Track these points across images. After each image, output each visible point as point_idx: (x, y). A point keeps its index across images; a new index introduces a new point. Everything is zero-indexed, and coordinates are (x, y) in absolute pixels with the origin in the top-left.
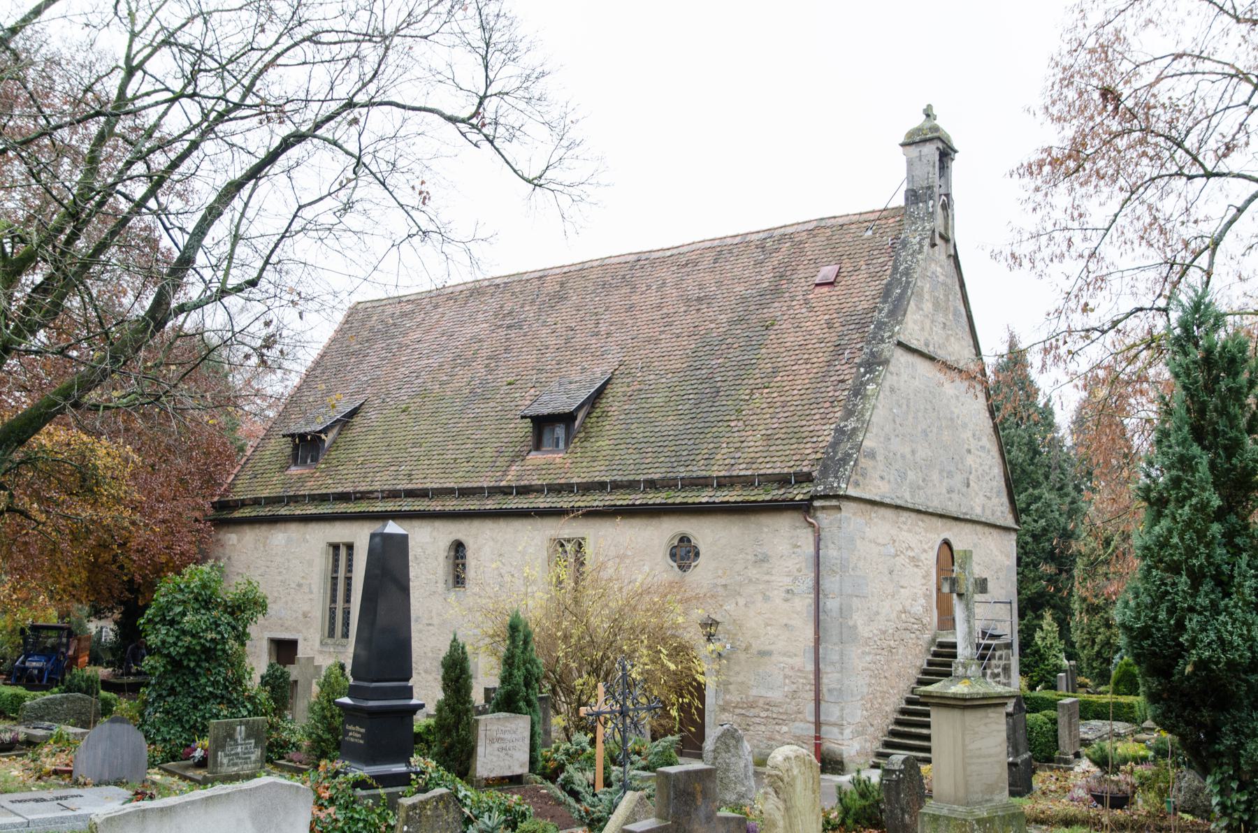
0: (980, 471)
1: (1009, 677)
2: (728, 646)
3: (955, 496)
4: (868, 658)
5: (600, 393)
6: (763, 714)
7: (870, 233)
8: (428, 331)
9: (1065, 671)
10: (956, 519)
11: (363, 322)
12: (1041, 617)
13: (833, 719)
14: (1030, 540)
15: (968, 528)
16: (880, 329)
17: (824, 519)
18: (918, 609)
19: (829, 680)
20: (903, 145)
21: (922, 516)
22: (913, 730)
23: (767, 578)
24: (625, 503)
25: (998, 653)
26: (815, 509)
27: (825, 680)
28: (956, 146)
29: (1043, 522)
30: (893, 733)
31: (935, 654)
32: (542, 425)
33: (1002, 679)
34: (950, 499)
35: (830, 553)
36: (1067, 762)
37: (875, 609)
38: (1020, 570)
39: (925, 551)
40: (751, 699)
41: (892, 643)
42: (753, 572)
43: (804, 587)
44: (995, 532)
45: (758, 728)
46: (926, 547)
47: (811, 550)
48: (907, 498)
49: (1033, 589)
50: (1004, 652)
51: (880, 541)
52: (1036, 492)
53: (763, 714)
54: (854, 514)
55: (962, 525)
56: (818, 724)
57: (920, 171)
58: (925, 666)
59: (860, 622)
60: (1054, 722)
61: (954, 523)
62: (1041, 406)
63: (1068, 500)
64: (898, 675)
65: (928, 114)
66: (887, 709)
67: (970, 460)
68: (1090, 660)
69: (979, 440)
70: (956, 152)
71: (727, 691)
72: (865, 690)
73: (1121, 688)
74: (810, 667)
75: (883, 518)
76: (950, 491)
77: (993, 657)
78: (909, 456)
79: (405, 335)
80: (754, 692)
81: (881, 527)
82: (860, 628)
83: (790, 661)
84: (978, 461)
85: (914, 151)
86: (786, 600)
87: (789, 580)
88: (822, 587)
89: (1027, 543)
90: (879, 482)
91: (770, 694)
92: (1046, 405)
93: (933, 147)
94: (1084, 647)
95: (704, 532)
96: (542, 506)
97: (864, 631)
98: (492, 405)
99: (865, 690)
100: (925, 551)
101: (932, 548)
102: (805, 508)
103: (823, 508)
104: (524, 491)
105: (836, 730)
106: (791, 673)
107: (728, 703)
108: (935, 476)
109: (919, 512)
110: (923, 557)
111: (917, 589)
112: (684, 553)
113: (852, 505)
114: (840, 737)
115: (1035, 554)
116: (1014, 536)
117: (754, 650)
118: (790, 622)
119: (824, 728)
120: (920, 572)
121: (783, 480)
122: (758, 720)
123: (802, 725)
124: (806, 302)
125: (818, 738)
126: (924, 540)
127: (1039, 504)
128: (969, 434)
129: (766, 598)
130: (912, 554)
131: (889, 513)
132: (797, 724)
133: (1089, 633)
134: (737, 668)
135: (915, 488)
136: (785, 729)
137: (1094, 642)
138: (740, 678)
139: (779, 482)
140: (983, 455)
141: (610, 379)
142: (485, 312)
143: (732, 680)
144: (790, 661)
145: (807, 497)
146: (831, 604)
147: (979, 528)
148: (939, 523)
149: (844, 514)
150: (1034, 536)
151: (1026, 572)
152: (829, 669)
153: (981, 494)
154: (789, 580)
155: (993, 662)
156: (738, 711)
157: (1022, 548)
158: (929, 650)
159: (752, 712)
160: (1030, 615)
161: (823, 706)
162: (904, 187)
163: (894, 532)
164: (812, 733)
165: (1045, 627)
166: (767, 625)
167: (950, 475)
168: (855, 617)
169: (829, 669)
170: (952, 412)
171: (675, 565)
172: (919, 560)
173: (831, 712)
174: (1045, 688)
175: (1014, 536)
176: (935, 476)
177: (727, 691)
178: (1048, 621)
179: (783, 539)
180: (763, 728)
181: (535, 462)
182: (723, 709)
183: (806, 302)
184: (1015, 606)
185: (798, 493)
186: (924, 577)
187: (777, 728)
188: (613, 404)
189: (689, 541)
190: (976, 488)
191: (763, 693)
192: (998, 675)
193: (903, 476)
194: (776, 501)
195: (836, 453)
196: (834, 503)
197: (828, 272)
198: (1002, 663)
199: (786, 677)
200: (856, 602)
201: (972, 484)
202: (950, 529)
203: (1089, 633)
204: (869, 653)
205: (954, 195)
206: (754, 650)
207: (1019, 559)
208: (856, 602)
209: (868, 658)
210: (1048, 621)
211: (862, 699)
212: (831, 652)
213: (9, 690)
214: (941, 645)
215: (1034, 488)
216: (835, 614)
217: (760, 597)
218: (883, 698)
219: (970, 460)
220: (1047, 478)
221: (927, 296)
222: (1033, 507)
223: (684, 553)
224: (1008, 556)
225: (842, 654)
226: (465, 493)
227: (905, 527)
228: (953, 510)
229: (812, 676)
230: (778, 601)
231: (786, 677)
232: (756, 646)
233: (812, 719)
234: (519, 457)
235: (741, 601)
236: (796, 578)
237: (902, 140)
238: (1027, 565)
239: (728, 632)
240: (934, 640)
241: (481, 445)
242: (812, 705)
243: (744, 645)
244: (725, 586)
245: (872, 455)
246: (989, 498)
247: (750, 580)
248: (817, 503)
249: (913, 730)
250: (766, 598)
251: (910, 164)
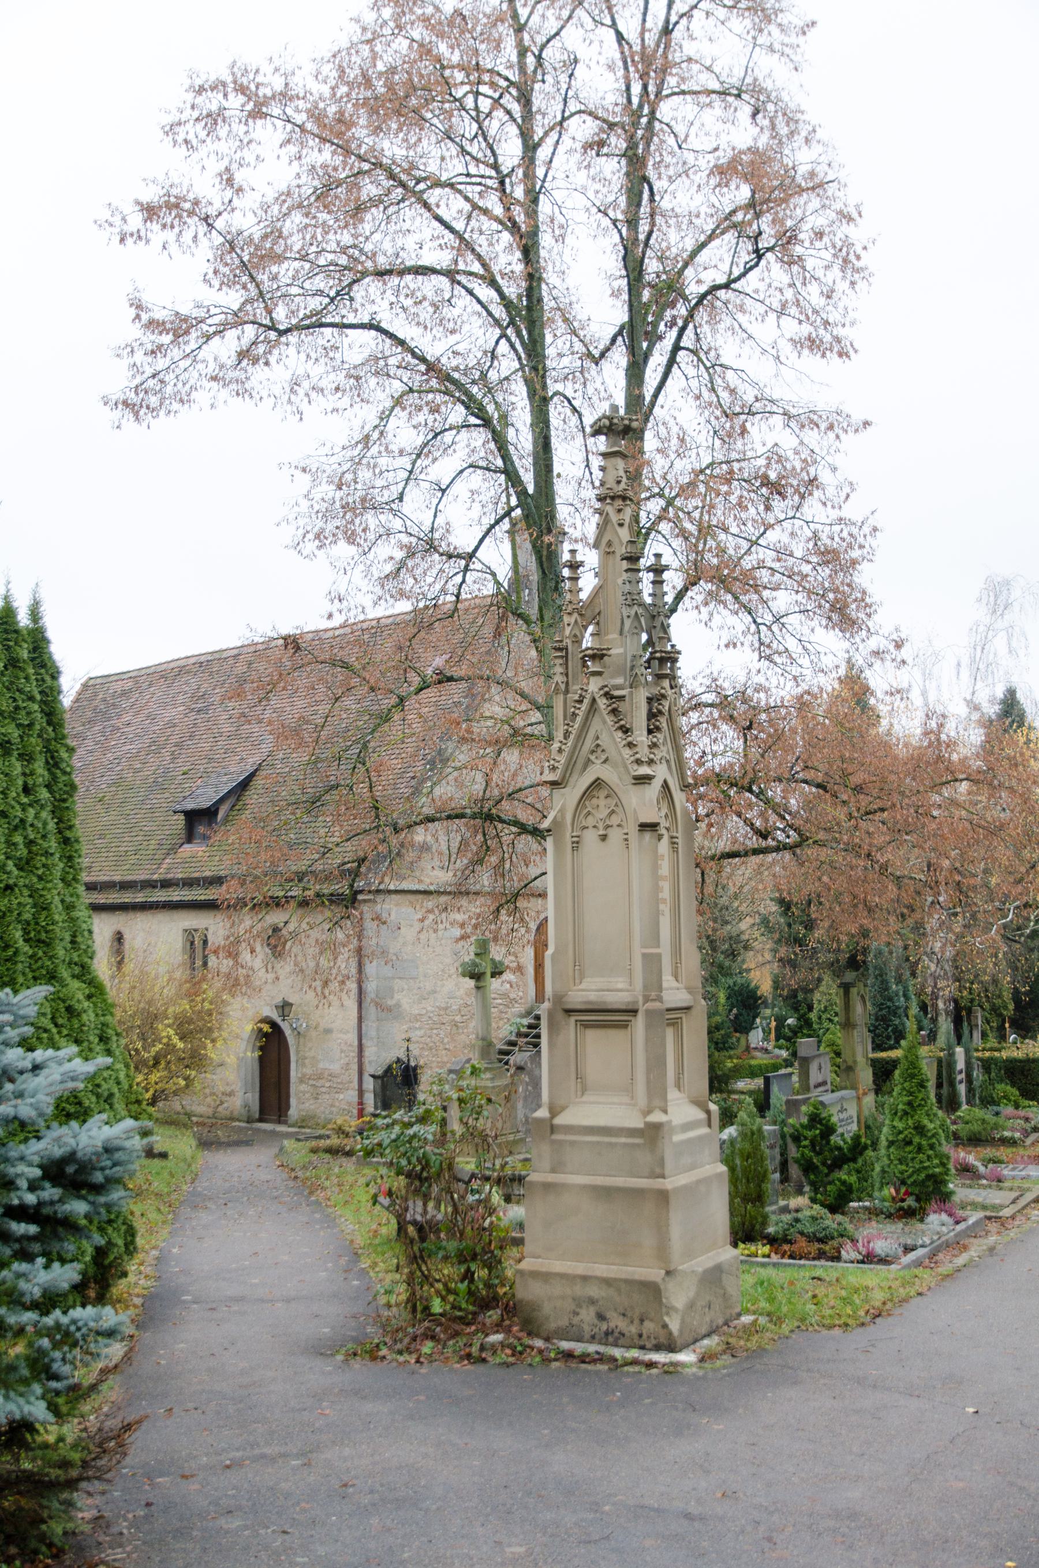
5: (244, 785)
8: (138, 713)
11: (91, 700)
32: (198, 820)
41: (458, 1018)
53: (328, 1084)
71: (304, 1065)
79: (119, 716)
80: (321, 1065)
83: (345, 1037)
96: (175, 899)
98: (167, 795)
103: (365, 901)
104: (166, 884)
107: (304, 1075)
136: (341, 1096)
138: (312, 1054)
141: (256, 770)
142: (186, 693)
144: (345, 1037)
156: (311, 1082)
159: (319, 1084)
181: (184, 855)
191: (327, 1066)
206: (321, 1029)
226: (125, 886)
231: (342, 1051)
234: (173, 850)
241: (148, 837)
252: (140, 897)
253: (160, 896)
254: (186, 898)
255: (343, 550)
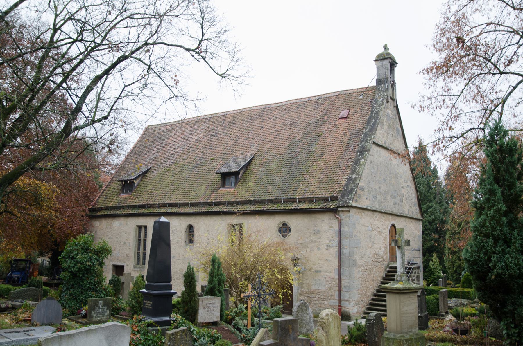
0: (407, 196)
1: (419, 281)
2: (303, 268)
3: (397, 206)
4: (361, 273)
5: (249, 163)
6: (317, 296)
7: (361, 97)
8: (178, 137)
9: (442, 278)
10: (397, 215)
11: (151, 134)
12: (432, 256)
13: (346, 298)
14: (427, 224)
15: (402, 219)
16: (366, 137)
17: (343, 216)
18: (381, 253)
19: (345, 282)
20: (375, 61)
21: (383, 214)
22: (379, 303)
23: (319, 240)
24: (260, 209)
25: (414, 271)
26: (339, 211)
27: (343, 282)
28: (397, 61)
29: (433, 217)
30: (371, 304)
31: (388, 271)
32: (226, 177)
33: (416, 282)
34: (395, 207)
35: (345, 230)
36: (442, 316)
37: (364, 253)
38: (424, 236)
39: (384, 229)
40: (312, 290)
41: (371, 267)
42: (313, 238)
43: (334, 244)
44: (413, 221)
45: (315, 302)
46: (385, 227)
47: (337, 228)
48: (377, 207)
49: (429, 244)
50: (416, 271)
51: (366, 225)
52: (430, 204)
53: (317, 296)
54: (355, 214)
55: (400, 218)
56: (340, 301)
57: (382, 71)
58: (384, 276)
59: (357, 259)
60: (437, 299)
61: (396, 217)
62: (432, 168)
63: (443, 207)
64: (373, 280)
65: (385, 47)
66: (369, 294)
67: (403, 191)
68: (452, 274)
69: (407, 183)
70: (397, 63)
71: (302, 287)
72: (359, 286)
73: (465, 285)
74: (337, 277)
75: (367, 215)
76: (395, 204)
77: (412, 272)
78: (378, 189)
80: (313, 287)
81: (366, 219)
82: (357, 261)
83: (328, 274)
84: (406, 191)
85: (379, 63)
86: (327, 249)
87: (328, 241)
88: (342, 244)
89: (426, 225)
90: (365, 200)
91: (320, 288)
92: (434, 168)
93: (387, 61)
94: (450, 268)
95: (293, 221)
96: (225, 210)
97: (359, 262)
98: (204, 168)
99: (359, 286)
100: (384, 229)
101: (387, 228)
102: (335, 211)
103: (342, 211)
104: (218, 204)
105: (347, 303)
106: (329, 280)
107: (303, 292)
108: (389, 198)
109: (382, 212)
110: (384, 231)
111: (381, 245)
112: (284, 230)
113: (354, 210)
114: (349, 306)
115: (430, 230)
116: (421, 223)
117: (313, 270)
118: (329, 259)
119: (342, 302)
120: (382, 238)
121: (326, 200)
122: (315, 299)
123: (333, 301)
124: (335, 125)
125: (340, 306)
126: (384, 224)
127: (432, 209)
128: (403, 180)
129: (319, 249)
130: (379, 230)
131: (369, 213)
132: (331, 300)
133: (452, 263)
134: (306, 278)
135: (380, 203)
136: (326, 302)
137: (454, 266)
138: (308, 282)
139: (324, 200)
140: (408, 189)
141: (254, 157)
142: (202, 129)
143: (304, 282)
144: (328, 274)
145: (336, 207)
146: (346, 251)
147: (407, 219)
148: (390, 217)
149: (351, 213)
150: (429, 222)
151: (426, 237)
152: (344, 278)
153: (408, 205)
154: (328, 241)
155: (412, 275)
156: (307, 295)
157: (424, 227)
158: (386, 270)
159: (313, 296)
160: (428, 255)
161: (342, 293)
162: (376, 78)
163: (371, 221)
164: (338, 304)
165: (434, 260)
166: (319, 260)
167: (395, 197)
168: (355, 256)
169: (344, 278)
170: (396, 171)
171: (281, 235)
172: (382, 233)
173: (345, 296)
174: (433, 285)
175: (421, 223)
176: (389, 198)
177: (302, 287)
178: (435, 258)
179: (326, 224)
180: (317, 302)
181: (222, 192)
182: (301, 294)
183: (335, 125)
184: (421, 251)
185: (332, 205)
186: (384, 240)
187: (323, 302)
188: (255, 168)
189: (287, 225)
190: (406, 203)
192: (414, 280)
193: (375, 198)
194: (323, 208)
195: (348, 188)
196: (347, 209)
197: (344, 113)
198: (416, 275)
199: (327, 281)
200: (356, 250)
201: (404, 201)
202: (395, 220)
203: (452, 263)
204: (361, 271)
205: (396, 81)
206: (313, 270)
207: (423, 232)
208: (356, 250)
209: (361, 273)
210: (435, 258)
211: (358, 290)
212: (345, 270)
213: (5, 286)
214: (391, 268)
215: (429, 202)
216: (347, 255)
217: (316, 248)
218: (367, 290)
219: (403, 191)
220: (435, 198)
221: (385, 123)
222: (429, 210)
223: (284, 230)
224: (418, 231)
225: (350, 272)
226: (193, 205)
227: (376, 219)
228: (396, 211)
229: (337, 281)
230: (324, 250)
231: (327, 281)
232: (314, 268)
233: (338, 298)
234: (216, 190)
235: (308, 250)
236: (331, 240)
237: (374, 58)
238: (426, 234)
239: (303, 263)
240: (388, 266)
242: (337, 293)
243: (309, 268)
244: (302, 243)
245: (362, 189)
246: (411, 207)
247: (312, 241)
248: (340, 209)
249: (379, 303)
250: (319, 249)
251: (378, 68)
252: (204, 210)
253: (181, 210)
254: (190, 211)
255: (426, 75)
